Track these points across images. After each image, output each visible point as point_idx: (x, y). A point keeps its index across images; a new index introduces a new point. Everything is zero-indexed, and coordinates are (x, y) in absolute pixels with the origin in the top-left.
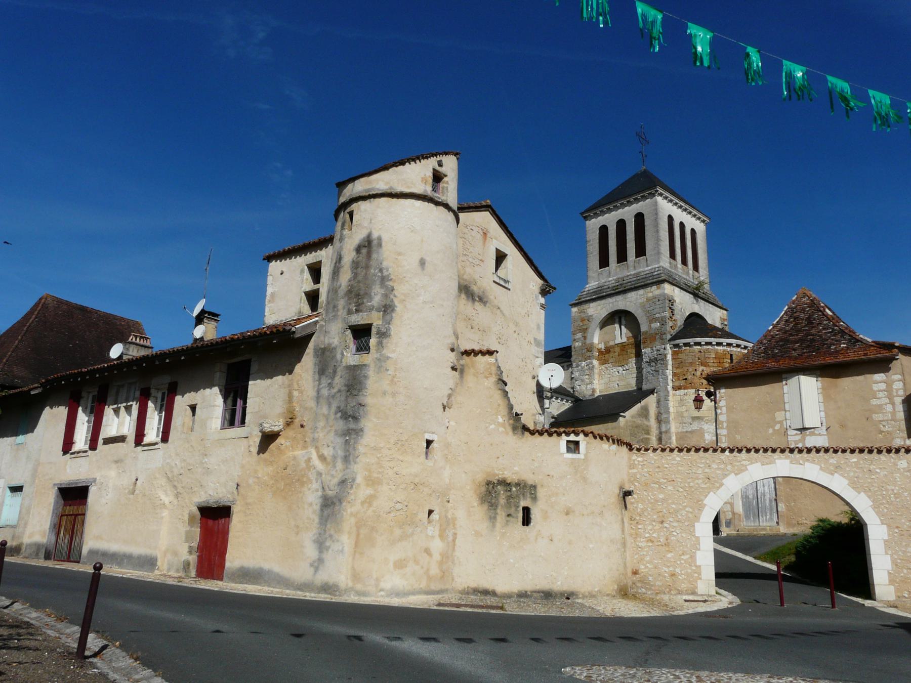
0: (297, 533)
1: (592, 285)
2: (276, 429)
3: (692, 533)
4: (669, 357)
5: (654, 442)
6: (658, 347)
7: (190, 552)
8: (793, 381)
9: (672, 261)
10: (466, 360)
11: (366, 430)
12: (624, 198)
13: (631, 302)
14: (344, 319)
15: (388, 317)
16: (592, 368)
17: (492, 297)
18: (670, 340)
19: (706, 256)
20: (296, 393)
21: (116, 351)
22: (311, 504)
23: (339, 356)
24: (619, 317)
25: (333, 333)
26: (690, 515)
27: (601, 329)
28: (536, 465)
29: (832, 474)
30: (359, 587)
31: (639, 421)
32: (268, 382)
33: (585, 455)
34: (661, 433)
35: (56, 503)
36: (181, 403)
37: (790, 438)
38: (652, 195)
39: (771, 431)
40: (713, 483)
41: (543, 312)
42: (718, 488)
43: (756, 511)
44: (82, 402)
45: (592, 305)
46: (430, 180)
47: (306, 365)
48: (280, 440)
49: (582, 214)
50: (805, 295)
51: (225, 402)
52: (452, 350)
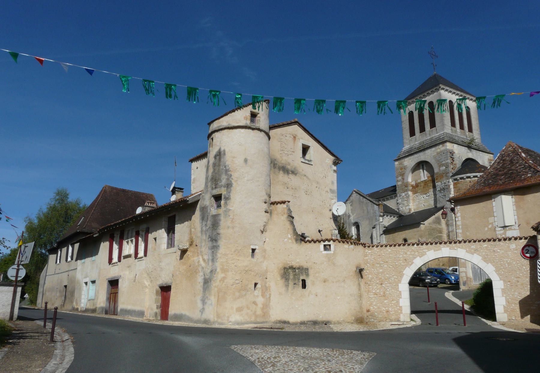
0: (195, 297)
1: (406, 147)
2: (185, 248)
3: (397, 289)
4: (452, 186)
5: (445, 238)
6: (445, 181)
7: (157, 308)
8: (498, 199)
9: (453, 128)
10: (273, 207)
11: (220, 246)
12: (421, 93)
13: (428, 156)
14: (211, 193)
15: (229, 190)
16: (408, 197)
17: (300, 171)
18: (452, 176)
19: (477, 122)
20: (193, 230)
21: (139, 210)
22: (200, 283)
23: (209, 211)
24: (422, 165)
25: (207, 201)
26: (396, 280)
27: (413, 173)
28: (308, 258)
29: (473, 254)
30: (220, 320)
31: (434, 226)
32: (182, 225)
33: (334, 251)
34: (449, 232)
35: (108, 288)
36: (151, 236)
37: (497, 233)
38: (437, 90)
39: (486, 229)
40: (408, 262)
41: (335, 174)
42: (411, 265)
43: (480, 276)
44: (115, 239)
46: (249, 118)
47: (197, 216)
48: (188, 253)
50: (510, 146)
51: (168, 235)
52: (265, 203)
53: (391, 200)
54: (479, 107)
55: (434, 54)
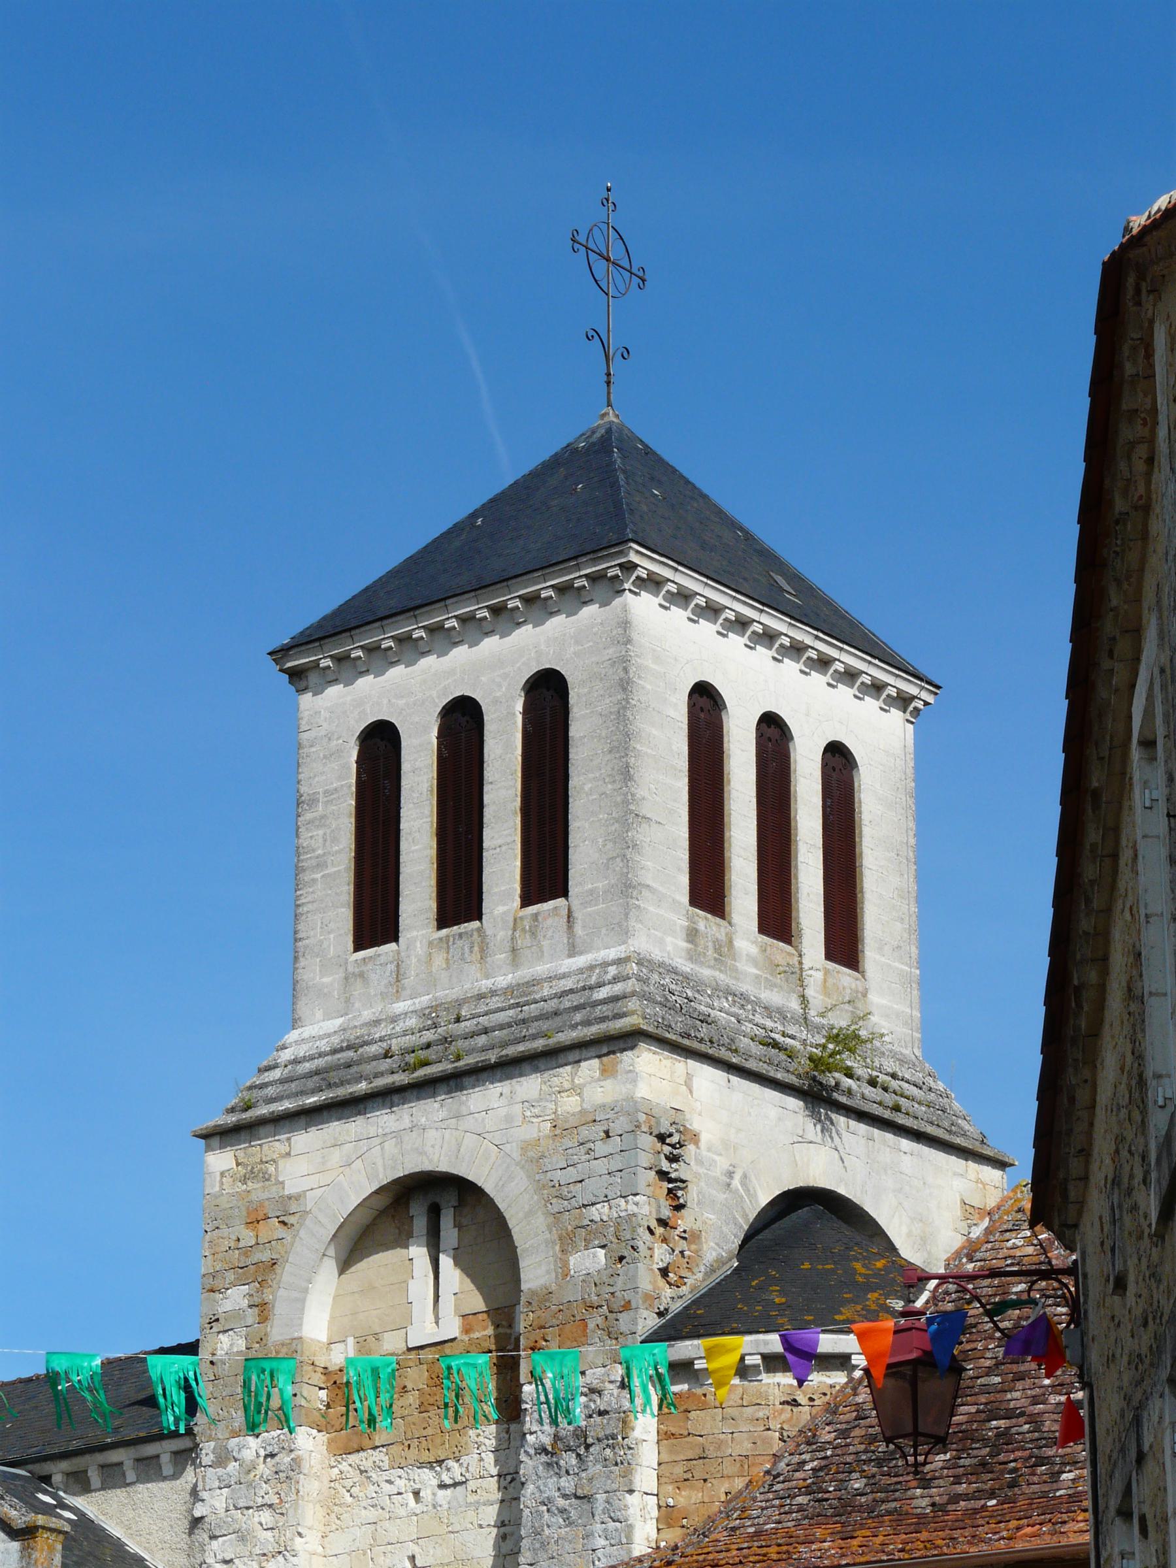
1: (315, 1031)
4: (645, 1427)
6: (594, 1376)
9: (705, 921)
12: (478, 588)
16: (288, 1475)
24: (428, 1205)
27: (345, 1265)
38: (608, 586)
45: (306, 1140)
49: (280, 654)
53: (145, 1491)
54: (926, 757)
55: (600, 266)
